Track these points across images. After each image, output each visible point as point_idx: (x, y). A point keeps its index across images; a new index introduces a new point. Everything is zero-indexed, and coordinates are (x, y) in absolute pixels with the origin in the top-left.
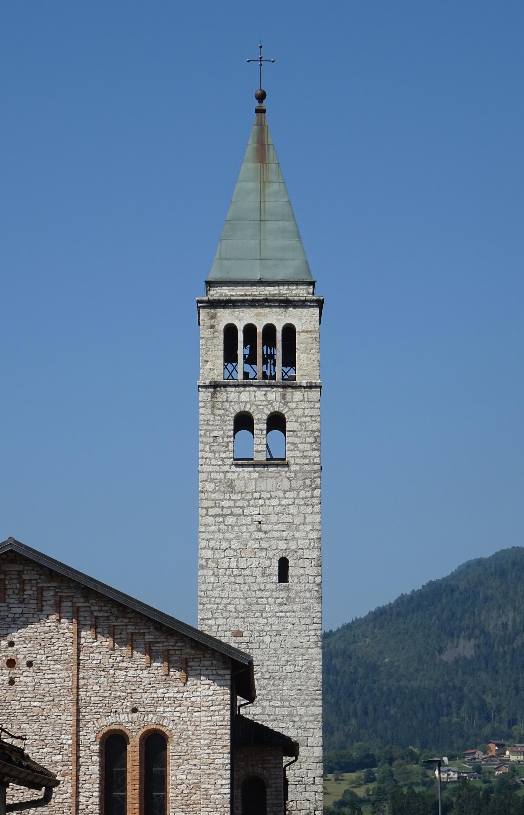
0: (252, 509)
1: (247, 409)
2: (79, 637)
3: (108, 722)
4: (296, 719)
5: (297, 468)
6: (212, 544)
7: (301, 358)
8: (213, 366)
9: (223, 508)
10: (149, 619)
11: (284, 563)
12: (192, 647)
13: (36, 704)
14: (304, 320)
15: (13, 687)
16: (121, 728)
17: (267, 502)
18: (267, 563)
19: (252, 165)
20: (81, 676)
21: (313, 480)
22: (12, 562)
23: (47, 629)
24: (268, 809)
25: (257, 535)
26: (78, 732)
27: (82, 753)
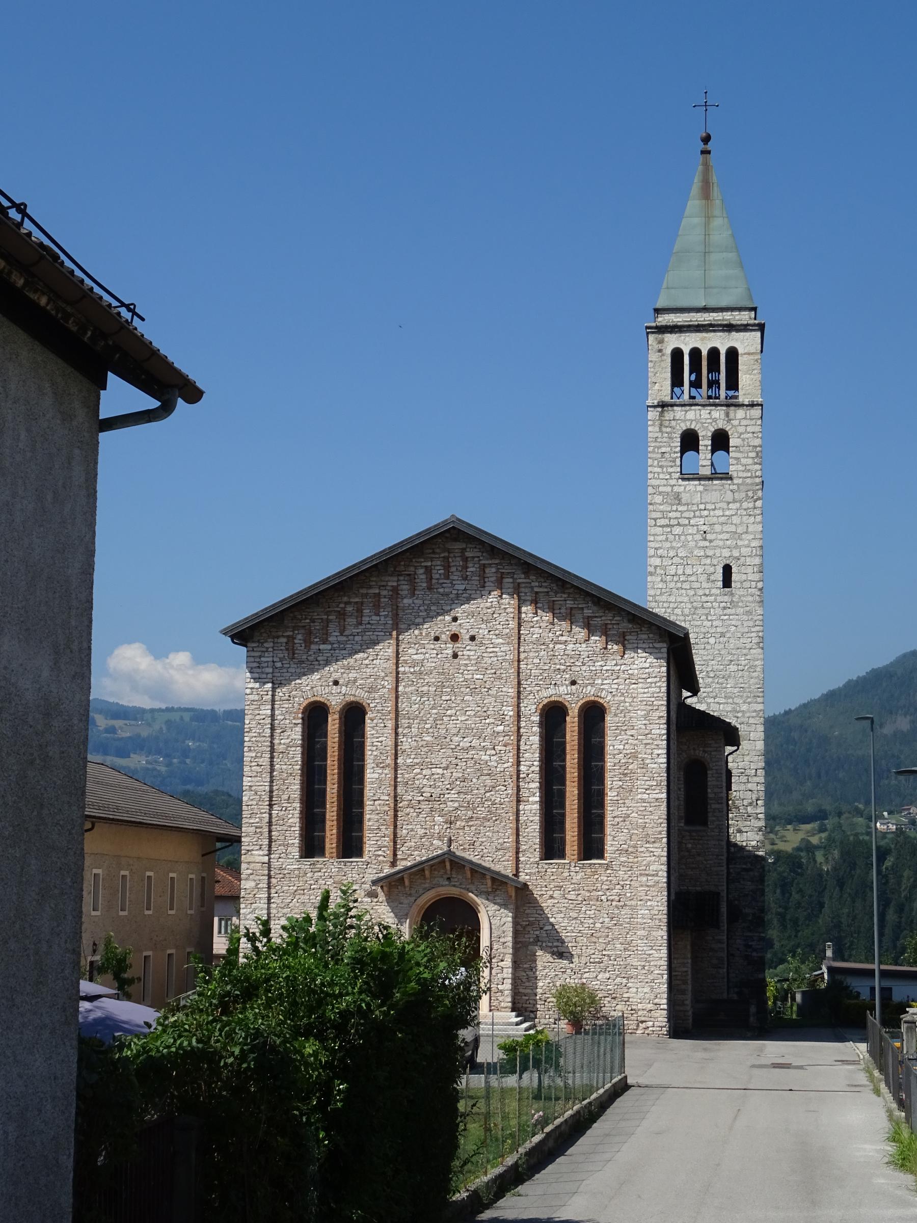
0: (698, 519)
1: (693, 427)
2: (520, 612)
3: (548, 694)
4: (740, 715)
5: (740, 481)
6: (660, 552)
7: (744, 379)
8: (660, 385)
9: (670, 518)
10: (588, 594)
11: (727, 570)
12: (629, 621)
13: (478, 677)
14: (746, 344)
15: (456, 661)
16: (560, 699)
17: (712, 513)
18: (712, 569)
19: (697, 202)
20: (522, 649)
21: (755, 492)
22: (456, 540)
23: (489, 605)
24: (709, 790)
25: (702, 544)
26: (519, 704)
27: (523, 724)
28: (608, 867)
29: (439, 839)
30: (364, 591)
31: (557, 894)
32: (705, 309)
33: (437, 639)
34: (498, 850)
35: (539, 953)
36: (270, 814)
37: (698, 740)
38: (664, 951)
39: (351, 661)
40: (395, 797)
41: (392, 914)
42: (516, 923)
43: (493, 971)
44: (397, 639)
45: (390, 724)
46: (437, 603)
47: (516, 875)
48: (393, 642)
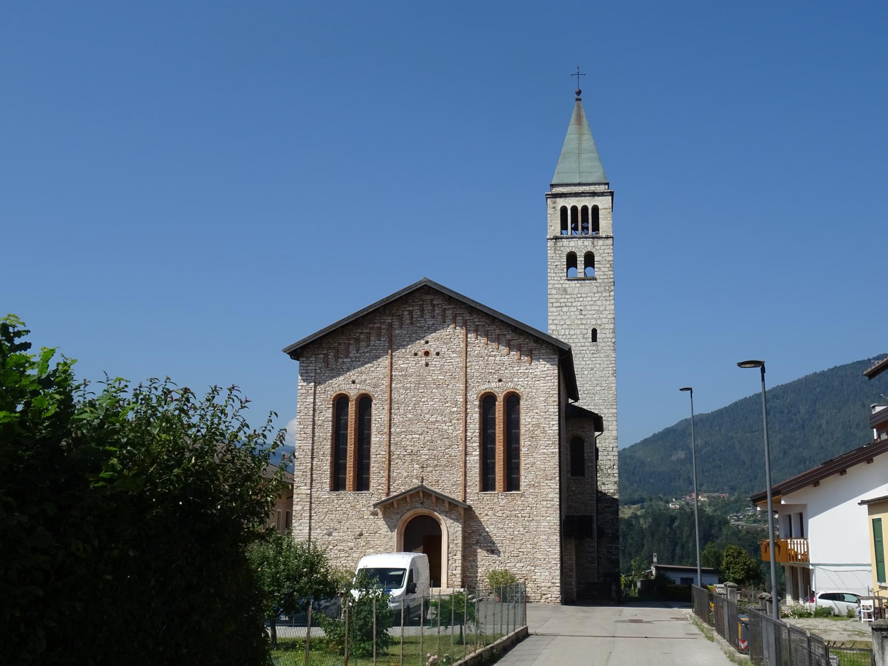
2: (467, 338)
3: (484, 388)
6: (555, 322)
8: (554, 228)
10: (509, 325)
11: (594, 332)
14: (603, 203)
18: (585, 331)
19: (574, 126)
21: (609, 287)
22: (427, 294)
25: (579, 317)
27: (469, 407)
28: (522, 495)
29: (417, 478)
31: (490, 513)
32: (580, 184)
33: (416, 354)
34: (453, 485)
35: (479, 550)
37: (578, 428)
38: (558, 549)
39: (363, 368)
42: (464, 531)
45: (387, 407)
46: (416, 333)
47: (465, 501)
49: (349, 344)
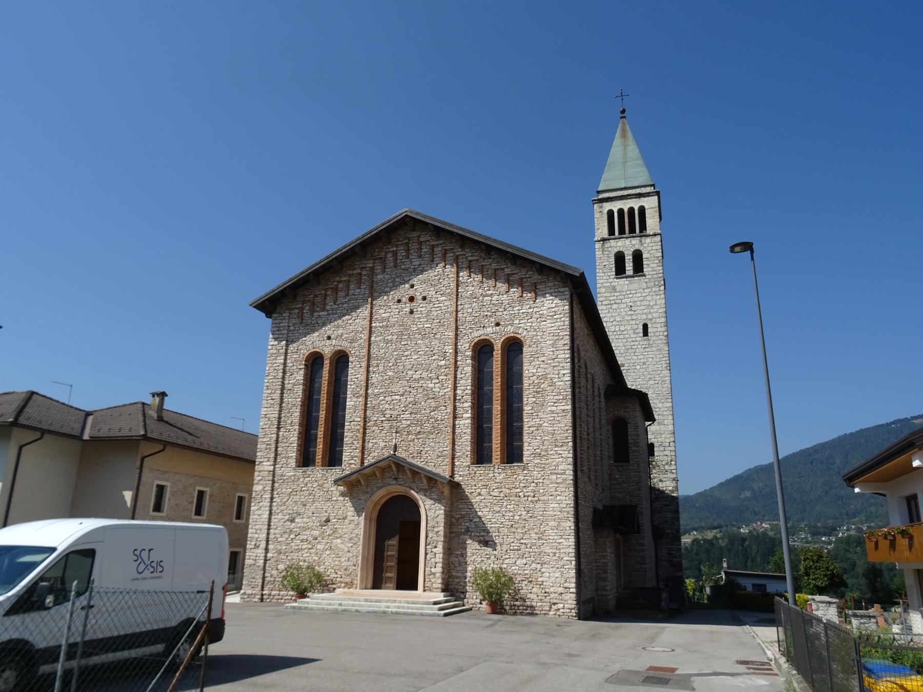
2: (458, 276)
3: (478, 334)
8: (602, 229)
11: (645, 327)
14: (650, 203)
21: (659, 282)
27: (459, 358)
30: (350, 272)
31: (484, 491)
32: (625, 188)
33: (399, 301)
34: (439, 457)
35: (469, 541)
36: (278, 435)
39: (340, 322)
40: (365, 418)
41: (352, 509)
43: (428, 557)
44: (372, 303)
45: (364, 364)
47: (452, 476)
48: (369, 306)
49: (326, 296)
